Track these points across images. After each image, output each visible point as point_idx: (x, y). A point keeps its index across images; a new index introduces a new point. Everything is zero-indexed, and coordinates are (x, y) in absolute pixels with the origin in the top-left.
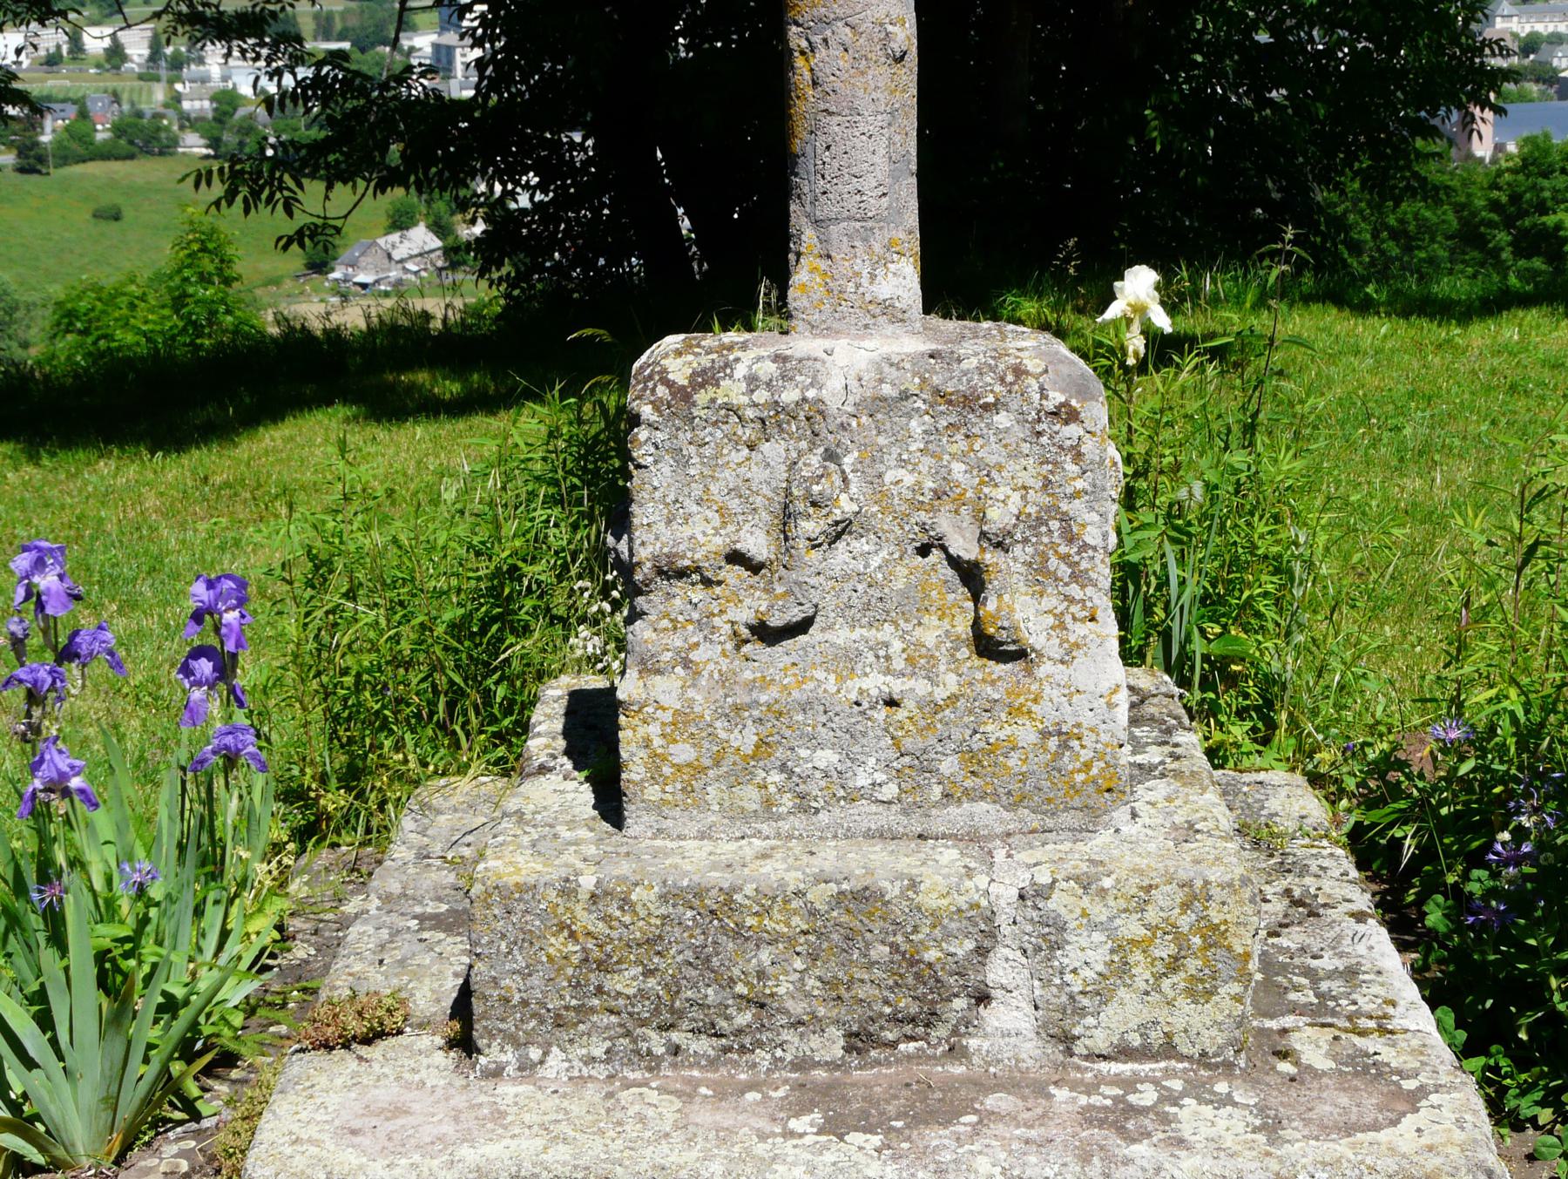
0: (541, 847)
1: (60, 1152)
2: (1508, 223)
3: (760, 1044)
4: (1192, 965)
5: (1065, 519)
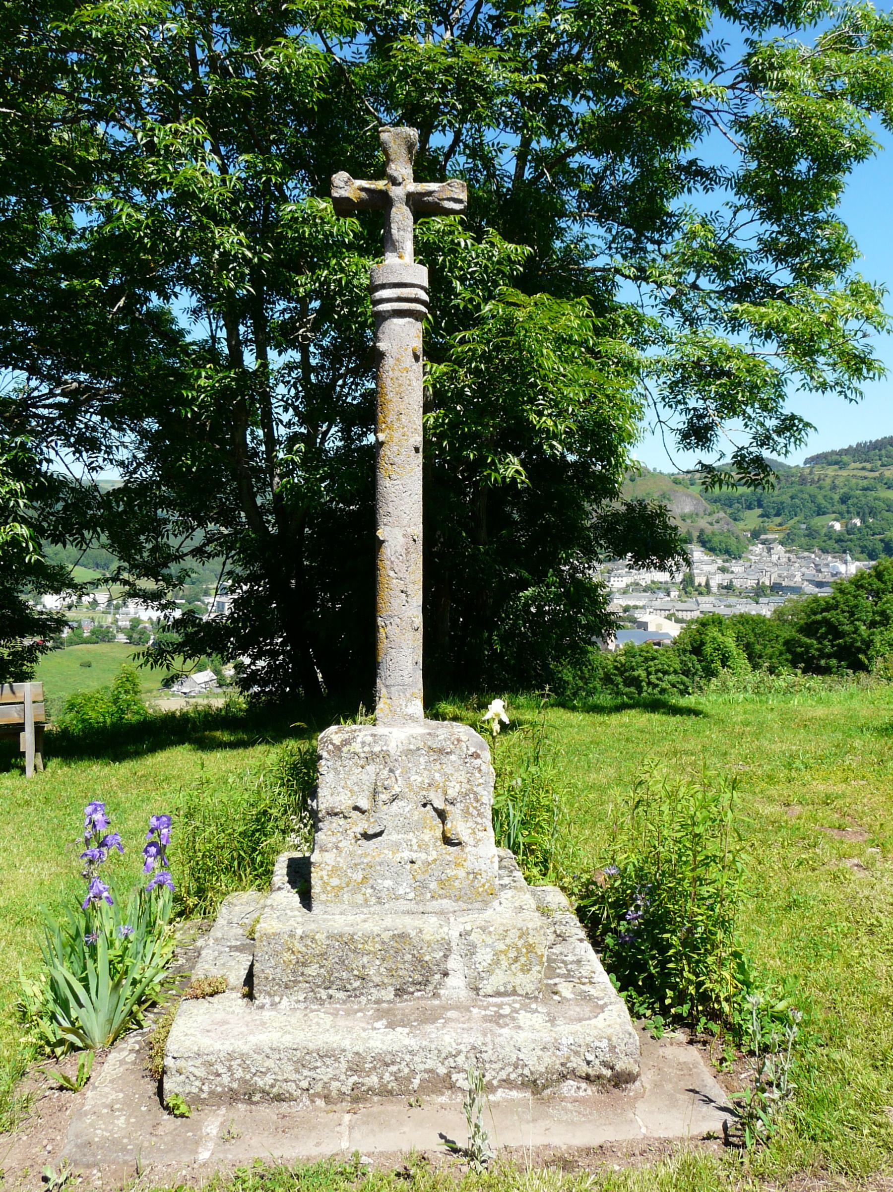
0: (281, 918)
1: (89, 1042)
2: (621, 674)
3: (362, 994)
4: (523, 959)
5: (475, 794)
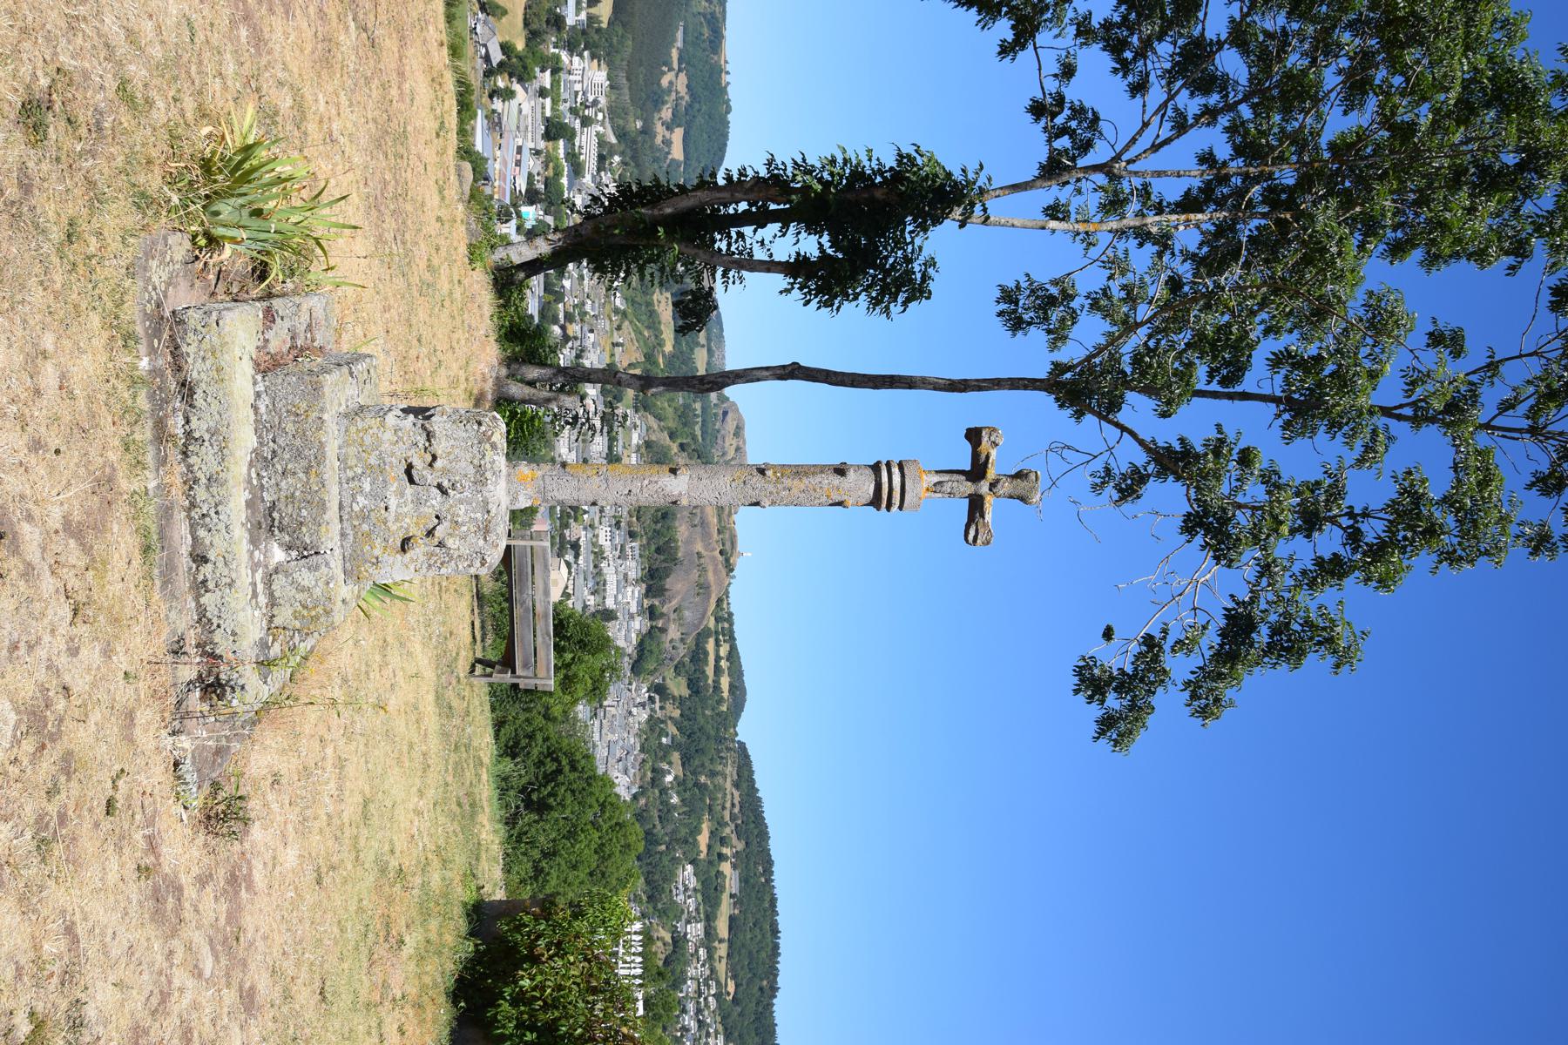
4: (305, 613)
